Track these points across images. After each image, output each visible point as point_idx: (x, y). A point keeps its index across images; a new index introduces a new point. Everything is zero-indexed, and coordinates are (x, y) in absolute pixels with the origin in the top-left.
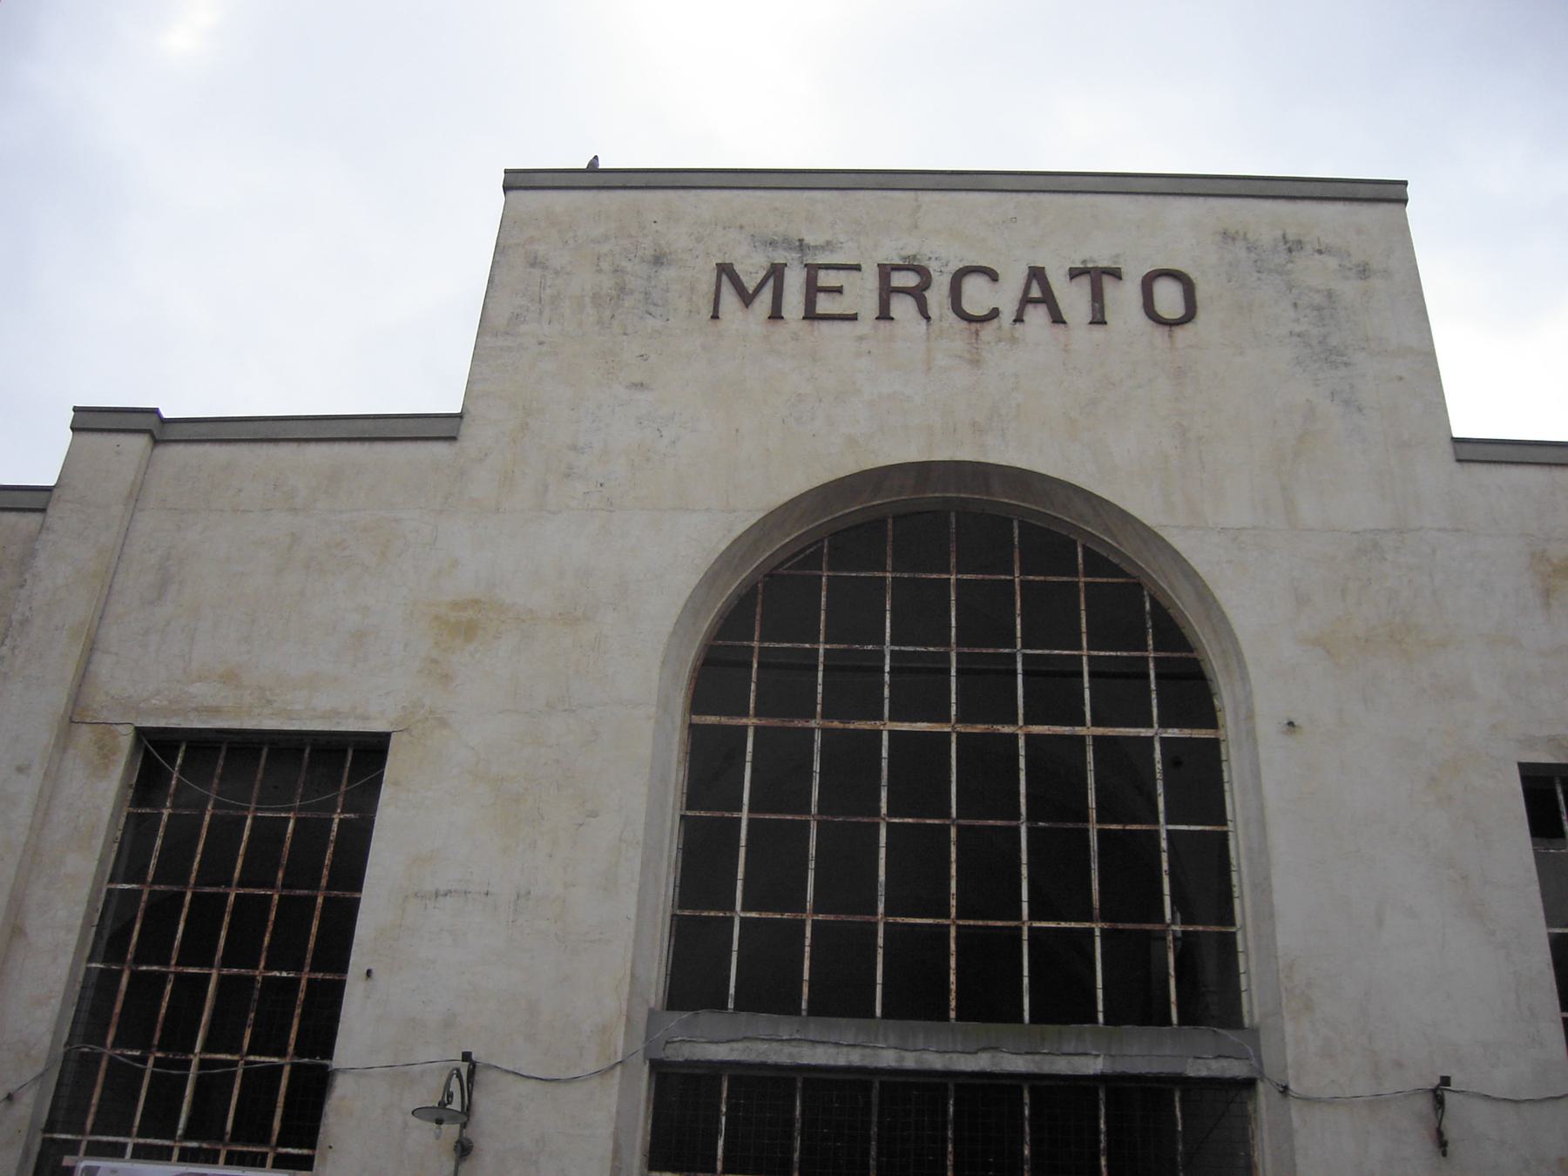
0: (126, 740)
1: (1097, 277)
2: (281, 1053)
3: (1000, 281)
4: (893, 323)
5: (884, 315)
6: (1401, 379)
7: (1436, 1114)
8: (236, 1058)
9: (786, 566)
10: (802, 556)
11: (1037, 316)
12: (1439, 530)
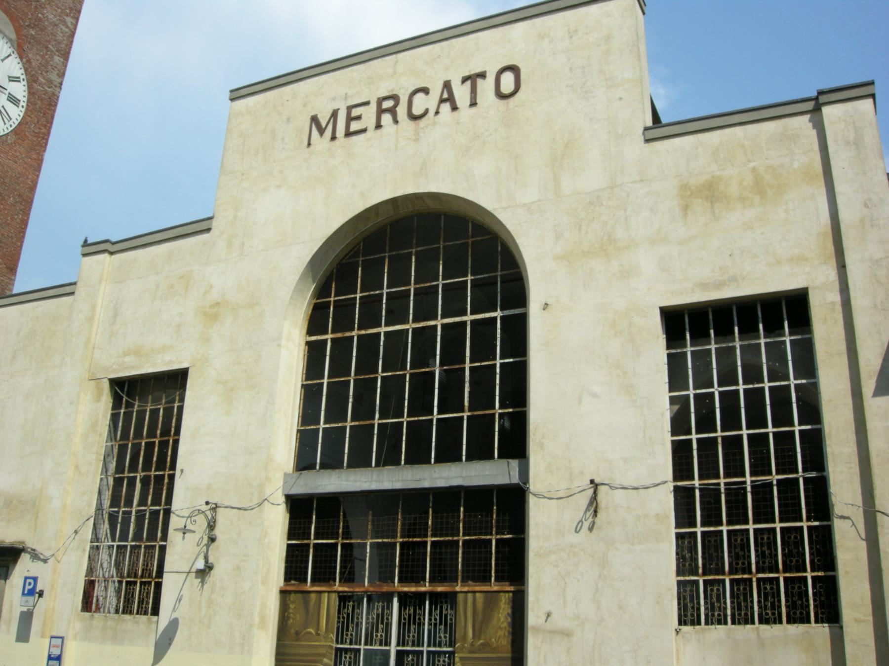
0: (106, 385)
1: (473, 79)
3: (429, 95)
4: (460, 83)
5: (379, 126)
6: (621, 99)
9: (346, 258)
10: (353, 252)
11: (446, 108)
12: (632, 183)
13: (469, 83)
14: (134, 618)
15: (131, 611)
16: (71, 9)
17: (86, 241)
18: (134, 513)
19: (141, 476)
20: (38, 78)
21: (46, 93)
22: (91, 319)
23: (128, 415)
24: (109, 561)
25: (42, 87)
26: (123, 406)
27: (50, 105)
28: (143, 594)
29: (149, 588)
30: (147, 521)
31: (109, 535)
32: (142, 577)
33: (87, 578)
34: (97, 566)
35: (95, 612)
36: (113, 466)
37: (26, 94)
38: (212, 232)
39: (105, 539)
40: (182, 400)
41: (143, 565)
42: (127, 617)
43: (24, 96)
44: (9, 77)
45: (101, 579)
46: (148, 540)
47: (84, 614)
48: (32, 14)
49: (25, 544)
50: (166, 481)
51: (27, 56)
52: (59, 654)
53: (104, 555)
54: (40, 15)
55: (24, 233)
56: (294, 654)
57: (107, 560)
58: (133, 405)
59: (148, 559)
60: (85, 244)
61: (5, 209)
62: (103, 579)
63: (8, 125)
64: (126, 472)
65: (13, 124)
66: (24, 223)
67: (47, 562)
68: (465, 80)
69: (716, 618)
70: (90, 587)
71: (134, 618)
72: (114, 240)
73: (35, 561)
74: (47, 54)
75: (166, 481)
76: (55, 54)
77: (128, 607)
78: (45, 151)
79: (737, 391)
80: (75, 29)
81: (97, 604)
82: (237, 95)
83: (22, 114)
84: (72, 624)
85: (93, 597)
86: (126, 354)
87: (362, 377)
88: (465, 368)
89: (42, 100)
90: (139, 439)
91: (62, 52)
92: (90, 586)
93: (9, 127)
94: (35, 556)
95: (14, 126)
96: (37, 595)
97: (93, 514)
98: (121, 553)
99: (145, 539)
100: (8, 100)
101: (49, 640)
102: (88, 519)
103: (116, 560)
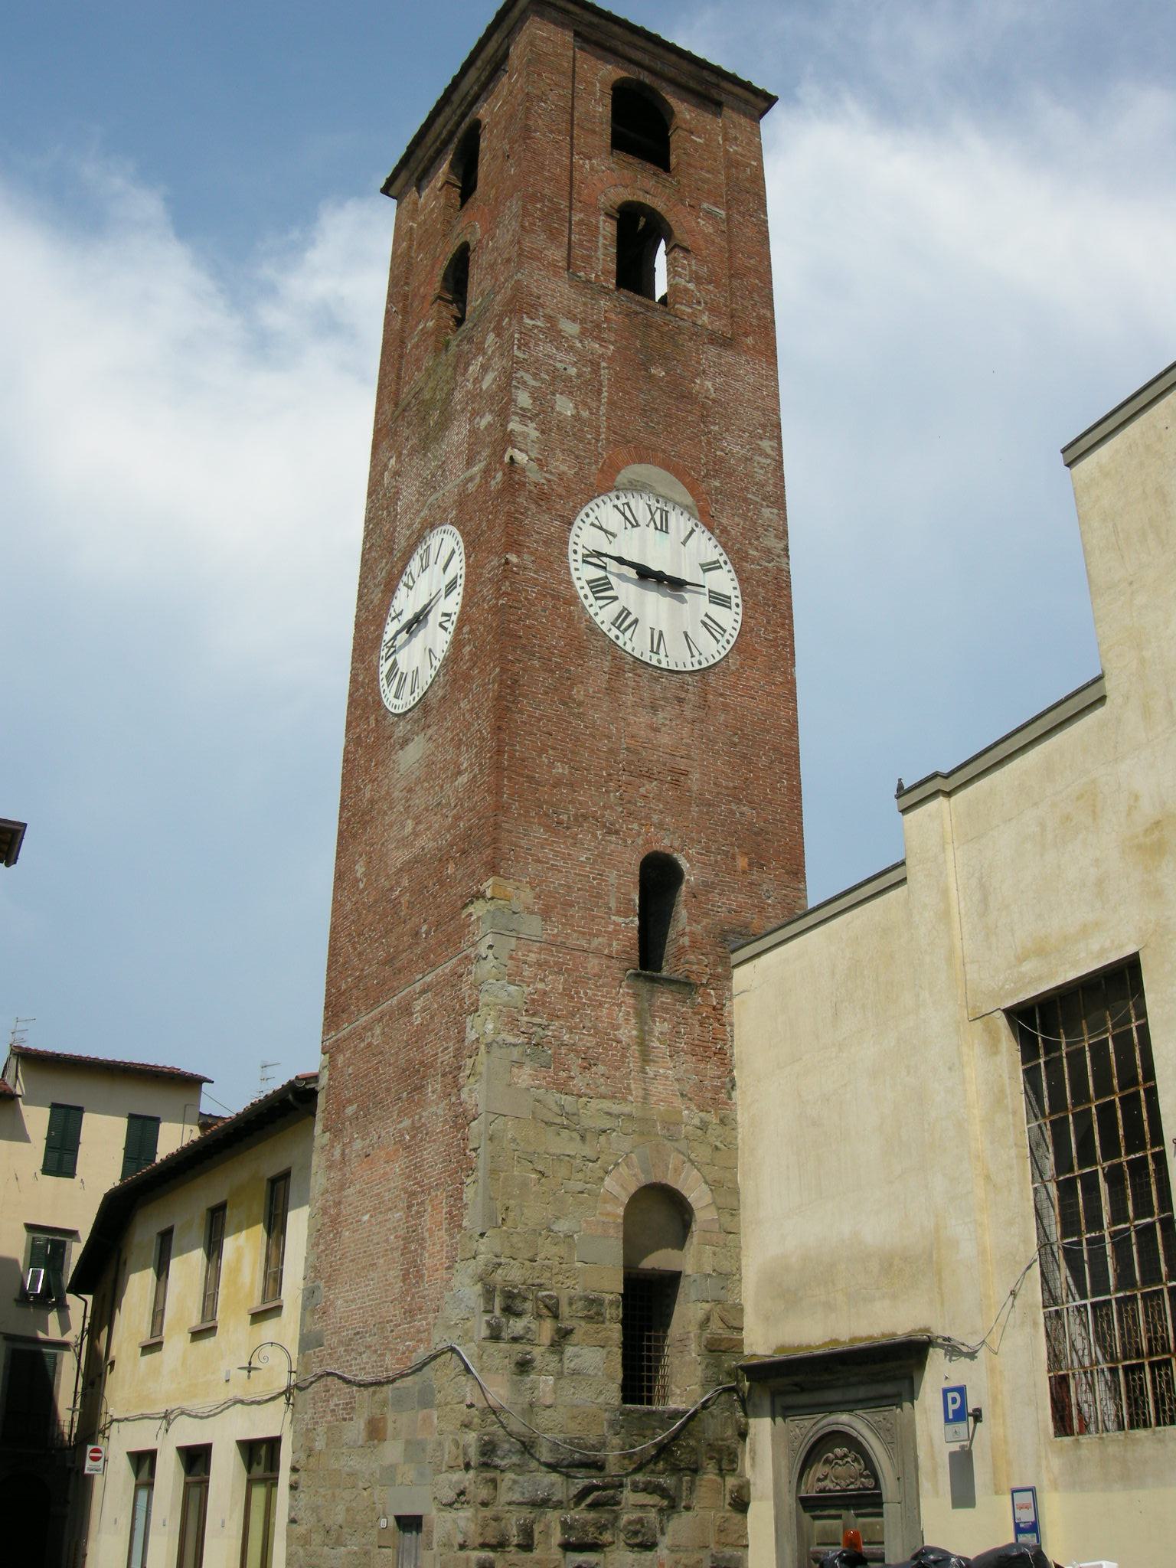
0: (1002, 1021)
2: (1151, 1214)
7: (137, 1473)
8: (1127, 1225)
14: (1154, 1433)
15: (1145, 1421)
16: (764, 426)
17: (900, 787)
18: (1108, 1239)
19: (1103, 1169)
20: (746, 552)
21: (767, 570)
22: (945, 915)
23: (1053, 1065)
24: (1084, 1335)
25: (758, 564)
26: (1042, 1051)
27: (780, 588)
28: (1161, 1387)
29: (1169, 1373)
30: (1134, 1248)
31: (1073, 1288)
32: (1151, 1353)
33: (1052, 1374)
34: (1065, 1347)
35: (1081, 1433)
36: (1049, 1163)
37: (736, 584)
38: (1108, 701)
39: (1067, 1296)
40: (1142, 1014)
41: (1148, 1330)
42: (1140, 1433)
43: (735, 588)
44: (702, 566)
45: (1078, 1370)
46: (1146, 1282)
47: (1061, 1441)
48: (706, 456)
49: (931, 1333)
50: (1152, 1167)
51: (720, 524)
52: (1033, 1519)
53: (1073, 1327)
54: (718, 453)
55: (800, 808)
57: (1080, 1335)
58: (1057, 1046)
59: (1153, 1318)
60: (902, 792)
61: (758, 778)
62: (1081, 1371)
63: (723, 642)
64: (1076, 1168)
65: (730, 638)
66: (796, 792)
67: (976, 1357)
70: (1061, 1388)
71: (1154, 1433)
72: (946, 770)
73: (954, 1358)
74: (748, 510)
75: (1152, 1167)
76: (762, 505)
77: (1138, 1415)
78: (793, 665)
80: (781, 456)
81: (1081, 1419)
82: (1075, 453)
83: (739, 618)
84: (1044, 1463)
85: (1070, 1406)
86: (1021, 960)
89: (764, 585)
90: (1085, 1103)
91: (772, 499)
92: (1060, 1387)
93: (726, 645)
94: (953, 1350)
95: (732, 641)
96: (971, 1419)
97: (1037, 1256)
98: (1101, 1316)
99: (1139, 1283)
100: (710, 602)
101: (1010, 1496)
102: (1029, 1267)
103: (1096, 1332)
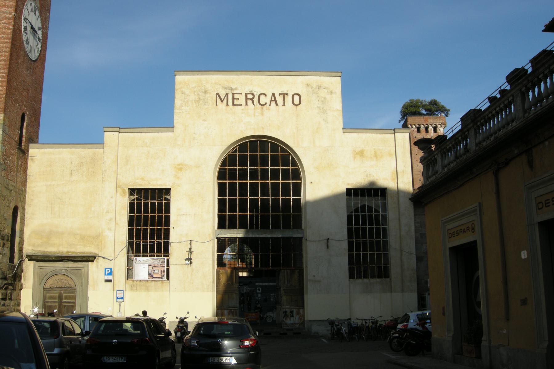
1: (284, 95)
5: (247, 104)
11: (273, 104)
13: (282, 96)
56: (79, 310)
68: (280, 94)
69: (359, 277)
79: (366, 215)
87: (242, 198)
88: (280, 198)
